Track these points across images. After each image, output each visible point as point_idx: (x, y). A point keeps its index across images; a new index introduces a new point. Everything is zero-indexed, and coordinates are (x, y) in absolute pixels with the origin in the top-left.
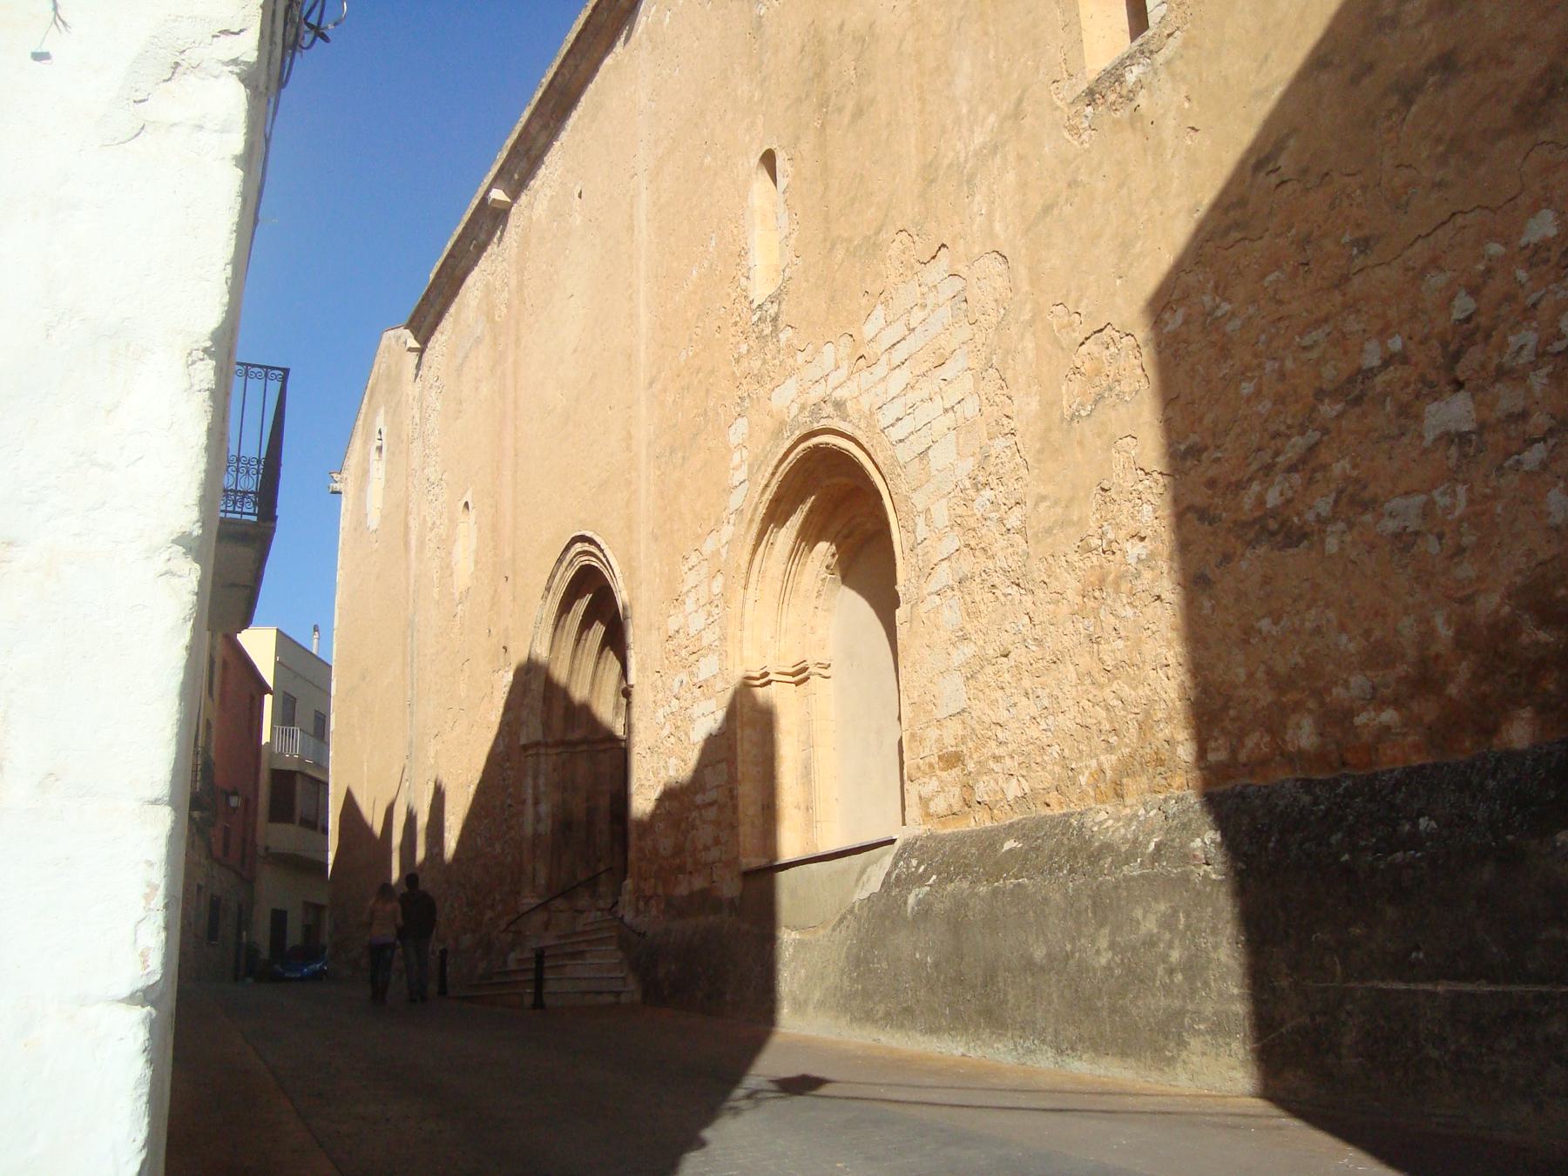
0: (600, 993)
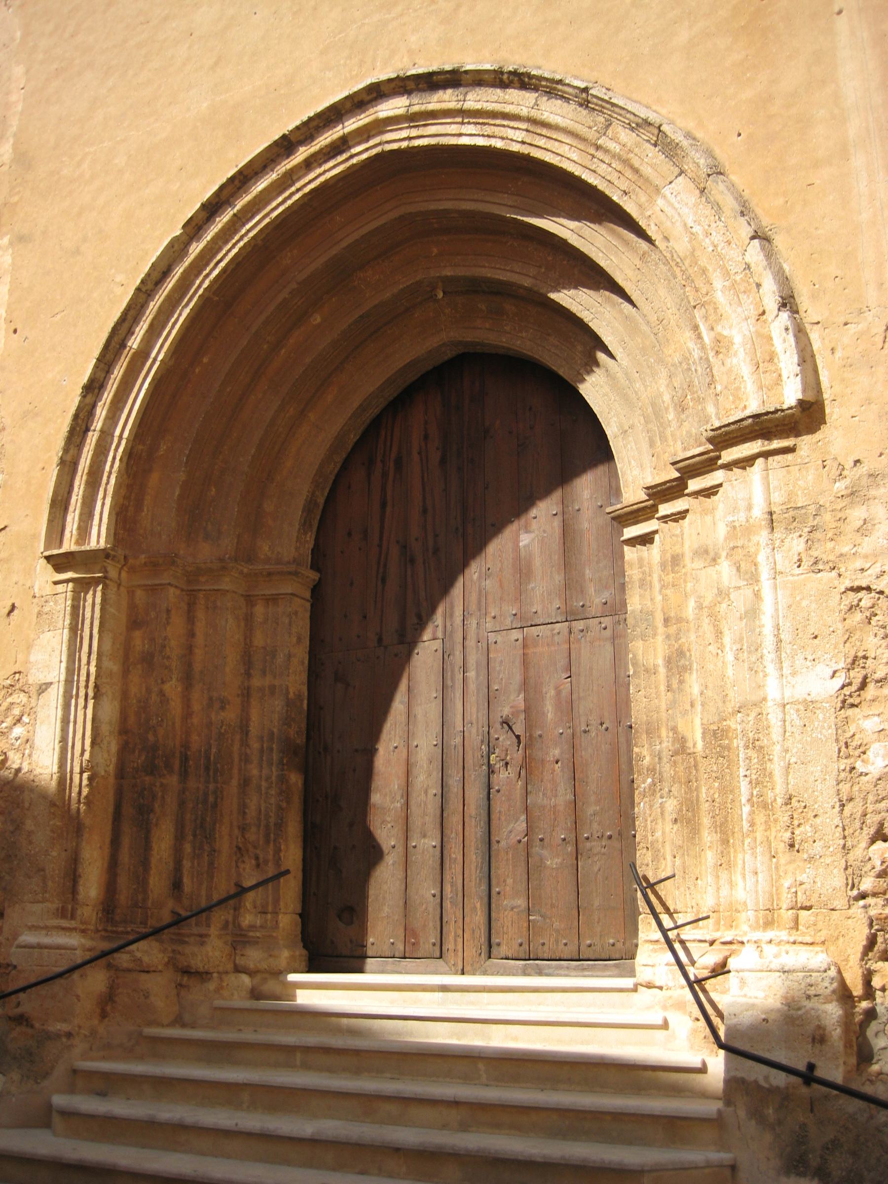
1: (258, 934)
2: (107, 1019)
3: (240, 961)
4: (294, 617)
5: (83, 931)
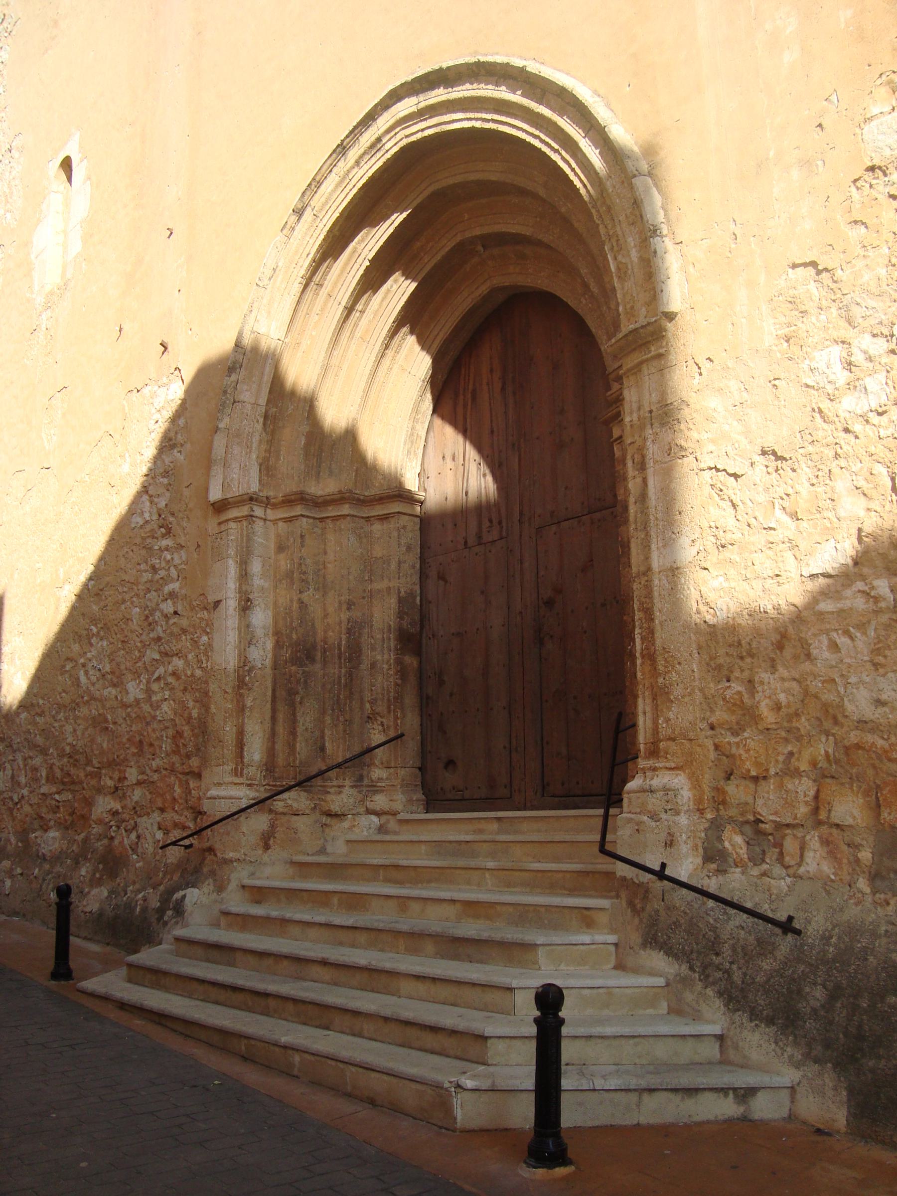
0: (692, 1091)
1: (383, 784)
2: (270, 850)
3: (370, 805)
4: (402, 530)
5: (249, 785)
